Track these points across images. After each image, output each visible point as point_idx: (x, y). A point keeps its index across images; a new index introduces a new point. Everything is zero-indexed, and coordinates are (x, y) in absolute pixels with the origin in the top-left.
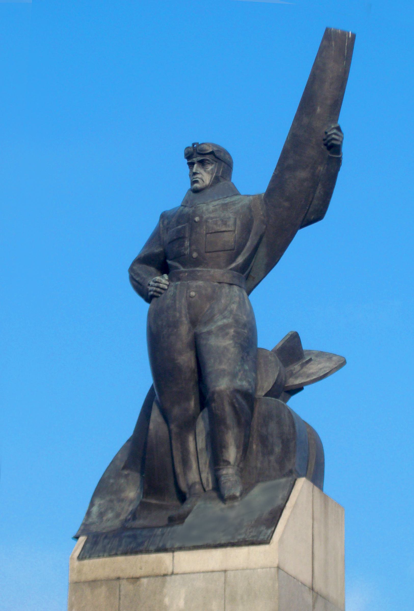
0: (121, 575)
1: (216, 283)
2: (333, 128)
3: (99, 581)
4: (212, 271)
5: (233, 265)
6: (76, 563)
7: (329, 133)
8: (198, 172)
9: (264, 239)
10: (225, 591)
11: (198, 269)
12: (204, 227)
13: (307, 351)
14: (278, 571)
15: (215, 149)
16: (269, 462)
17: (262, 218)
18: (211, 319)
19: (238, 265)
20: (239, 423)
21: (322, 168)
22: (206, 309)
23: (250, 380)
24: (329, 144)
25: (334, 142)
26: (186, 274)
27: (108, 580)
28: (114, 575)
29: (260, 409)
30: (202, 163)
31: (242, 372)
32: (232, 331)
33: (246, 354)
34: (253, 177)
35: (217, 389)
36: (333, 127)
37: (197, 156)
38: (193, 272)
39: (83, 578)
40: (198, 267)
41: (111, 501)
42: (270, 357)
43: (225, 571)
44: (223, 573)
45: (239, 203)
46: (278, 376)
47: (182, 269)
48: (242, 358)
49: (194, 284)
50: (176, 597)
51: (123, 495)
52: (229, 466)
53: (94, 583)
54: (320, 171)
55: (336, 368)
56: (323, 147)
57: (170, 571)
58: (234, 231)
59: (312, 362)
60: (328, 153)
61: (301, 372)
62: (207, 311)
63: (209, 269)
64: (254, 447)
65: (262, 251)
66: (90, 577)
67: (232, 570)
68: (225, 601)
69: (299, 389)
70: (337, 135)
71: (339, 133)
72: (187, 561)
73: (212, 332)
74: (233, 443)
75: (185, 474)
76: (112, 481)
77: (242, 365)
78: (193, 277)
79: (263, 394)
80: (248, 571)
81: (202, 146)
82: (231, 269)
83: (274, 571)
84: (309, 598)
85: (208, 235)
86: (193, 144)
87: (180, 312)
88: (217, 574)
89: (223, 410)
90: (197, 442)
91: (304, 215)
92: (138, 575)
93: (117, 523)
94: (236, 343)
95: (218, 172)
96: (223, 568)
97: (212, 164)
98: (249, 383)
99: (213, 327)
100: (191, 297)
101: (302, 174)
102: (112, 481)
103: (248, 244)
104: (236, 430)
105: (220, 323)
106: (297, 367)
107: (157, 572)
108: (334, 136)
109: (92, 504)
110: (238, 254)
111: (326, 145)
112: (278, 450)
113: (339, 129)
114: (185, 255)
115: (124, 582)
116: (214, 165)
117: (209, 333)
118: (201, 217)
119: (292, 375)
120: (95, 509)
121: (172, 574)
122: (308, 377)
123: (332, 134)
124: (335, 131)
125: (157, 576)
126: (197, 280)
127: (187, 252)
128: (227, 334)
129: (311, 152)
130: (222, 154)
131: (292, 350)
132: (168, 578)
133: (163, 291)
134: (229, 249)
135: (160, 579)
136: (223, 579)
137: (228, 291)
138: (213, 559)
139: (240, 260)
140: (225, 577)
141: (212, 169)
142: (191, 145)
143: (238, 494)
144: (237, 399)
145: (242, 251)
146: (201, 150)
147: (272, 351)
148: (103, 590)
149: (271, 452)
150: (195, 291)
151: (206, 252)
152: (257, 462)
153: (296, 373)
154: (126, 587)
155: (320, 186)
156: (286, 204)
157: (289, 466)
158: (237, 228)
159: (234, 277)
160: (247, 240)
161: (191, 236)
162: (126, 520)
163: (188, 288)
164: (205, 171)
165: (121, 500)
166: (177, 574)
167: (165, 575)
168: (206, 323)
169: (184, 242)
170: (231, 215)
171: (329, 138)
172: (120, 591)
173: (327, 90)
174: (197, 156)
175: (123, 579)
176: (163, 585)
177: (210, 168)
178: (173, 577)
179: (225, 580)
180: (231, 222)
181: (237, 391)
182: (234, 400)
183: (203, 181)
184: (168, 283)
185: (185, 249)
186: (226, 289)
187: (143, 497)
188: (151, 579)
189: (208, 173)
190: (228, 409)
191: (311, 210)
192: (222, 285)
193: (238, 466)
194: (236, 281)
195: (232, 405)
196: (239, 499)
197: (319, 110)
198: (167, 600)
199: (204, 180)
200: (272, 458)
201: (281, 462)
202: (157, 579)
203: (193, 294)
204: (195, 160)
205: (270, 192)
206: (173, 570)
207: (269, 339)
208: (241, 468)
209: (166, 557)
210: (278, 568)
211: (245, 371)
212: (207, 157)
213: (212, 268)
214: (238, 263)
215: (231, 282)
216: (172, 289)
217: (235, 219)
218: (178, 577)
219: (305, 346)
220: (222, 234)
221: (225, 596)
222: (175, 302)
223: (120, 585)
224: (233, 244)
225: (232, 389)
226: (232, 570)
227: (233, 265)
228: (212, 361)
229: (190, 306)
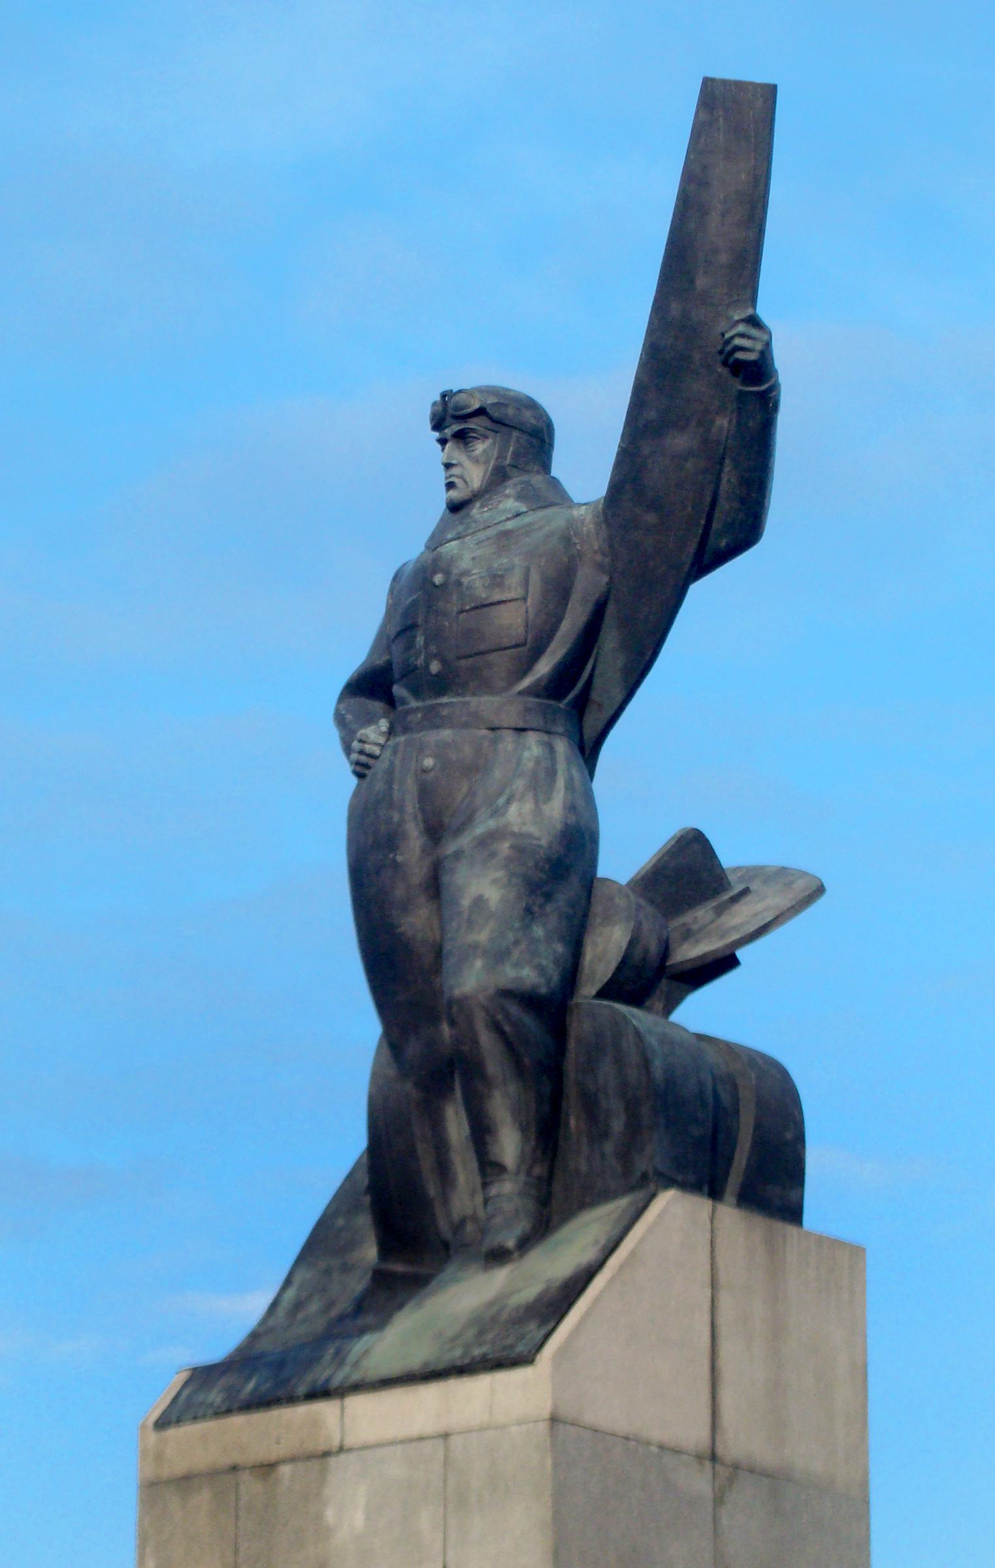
0: (236, 1458)
1: (484, 732)
2: (738, 322)
3: (196, 1476)
4: (474, 701)
5: (526, 682)
6: (153, 1437)
7: (727, 336)
8: (454, 462)
9: (611, 609)
10: (445, 1482)
11: (445, 700)
12: (455, 598)
13: (737, 869)
14: (552, 1428)
15: (491, 400)
16: (603, 1156)
17: (599, 558)
18: (469, 820)
19: (539, 680)
20: (519, 1070)
21: (725, 423)
22: (459, 798)
23: (544, 962)
24: (731, 360)
25: (740, 355)
26: (420, 716)
27: (213, 1474)
28: (224, 1461)
29: (579, 1028)
30: (462, 437)
31: (523, 946)
32: (504, 848)
33: (540, 900)
34: (585, 465)
35: (457, 992)
36: (736, 318)
37: (456, 420)
38: (433, 707)
39: (166, 1472)
40: (444, 695)
41: (327, 1272)
42: (617, 900)
43: (446, 1436)
44: (441, 1441)
45: (541, 528)
46: (632, 943)
47: (414, 704)
48: (528, 910)
49: (432, 737)
50: (350, 1508)
51: (356, 1255)
52: (505, 1176)
53: (186, 1482)
54: (721, 428)
55: (793, 907)
56: (720, 369)
57: (336, 1443)
58: (525, 599)
59: (748, 898)
60: (737, 386)
61: (713, 926)
62: (462, 801)
63: (467, 699)
64: (573, 1122)
65: (609, 640)
66: (179, 1469)
67: (460, 1433)
68: (445, 1507)
69: (725, 963)
70: (749, 337)
71: (754, 332)
72: (368, 1417)
73: (463, 852)
74: (509, 1119)
75: (446, 1200)
76: (340, 1222)
77: (526, 927)
78: (433, 720)
79: (594, 992)
80: (491, 1432)
81: (457, 398)
82: (520, 693)
83: (543, 1427)
84: (700, 1483)
85: (461, 616)
86: (444, 396)
87: (401, 810)
88: (429, 1444)
89: (475, 1042)
90: (456, 1124)
91: (697, 539)
92: (273, 1456)
93: (319, 1325)
94: (512, 875)
95: (501, 456)
96: (442, 1427)
97: (486, 437)
98: (541, 970)
99: (465, 841)
100: (425, 771)
101: (680, 442)
102: (340, 1222)
103: (565, 626)
104: (513, 1088)
105: (479, 830)
106: (702, 914)
107: (310, 1447)
108: (738, 341)
109: (288, 1282)
110: (537, 653)
111: (725, 363)
112: (618, 1124)
113: (754, 321)
114: (416, 668)
115: (245, 1476)
116: (490, 441)
117: (458, 855)
118: (447, 573)
119: (688, 934)
120: (291, 1294)
121: (341, 1449)
122: (722, 937)
123: (732, 338)
124: (741, 328)
125: (310, 1457)
126: (438, 727)
127: (420, 661)
128: (493, 855)
129: (698, 387)
130: (511, 411)
131: (688, 872)
132: (333, 1461)
133: (371, 762)
134: (514, 643)
135: (315, 1464)
136: (441, 1454)
137: (510, 747)
138: (423, 1407)
139: (544, 667)
140: (447, 1449)
141: (485, 451)
142: (438, 398)
143: (511, 1243)
144: (507, 1016)
145: (546, 646)
146: (457, 408)
147: (628, 884)
148: (203, 1498)
149: (605, 1134)
150: (435, 756)
151: (459, 658)
152: (580, 1157)
153: (700, 930)
154: (250, 1487)
155: (728, 465)
156: (651, 518)
157: (642, 1164)
158: (531, 590)
159: (527, 710)
160: (560, 620)
161: (426, 620)
162: (341, 1318)
163: (421, 749)
164: (469, 457)
165: (346, 1269)
166: (350, 1450)
167: (326, 1454)
168: (458, 831)
169: (415, 637)
170: (517, 561)
171: (729, 348)
172: (237, 1499)
173: (718, 230)
174: (456, 420)
175: (245, 1468)
176: (323, 1475)
177: (480, 447)
178: (342, 1457)
179: (445, 1456)
180: (514, 579)
181: (506, 993)
182: (500, 1017)
183: (466, 482)
184: (382, 740)
185: (417, 655)
186: (508, 741)
187: (385, 1251)
188: (300, 1465)
189: (476, 461)
190: (487, 1040)
191: (716, 525)
192: (499, 732)
193: (529, 1173)
194: (537, 721)
195: (496, 1027)
196: (516, 1255)
197: (701, 282)
198: (330, 1515)
199: (468, 479)
200: (609, 1147)
201: (625, 1155)
202: (309, 1464)
203: (429, 762)
204: (448, 432)
205: (615, 489)
206: (342, 1440)
207: (625, 853)
208: (539, 1178)
209: (326, 1409)
210: (554, 1420)
211: (534, 941)
212: (472, 424)
213: (474, 694)
214: (538, 676)
215: (521, 725)
216: (388, 753)
217: (528, 570)
218: (352, 1457)
219: (731, 854)
220: (493, 611)
221: (445, 1499)
222: (390, 788)
223: (237, 1484)
224: (521, 630)
225: (491, 991)
226: (460, 1433)
227: (526, 682)
228: (454, 924)
229: (425, 793)
